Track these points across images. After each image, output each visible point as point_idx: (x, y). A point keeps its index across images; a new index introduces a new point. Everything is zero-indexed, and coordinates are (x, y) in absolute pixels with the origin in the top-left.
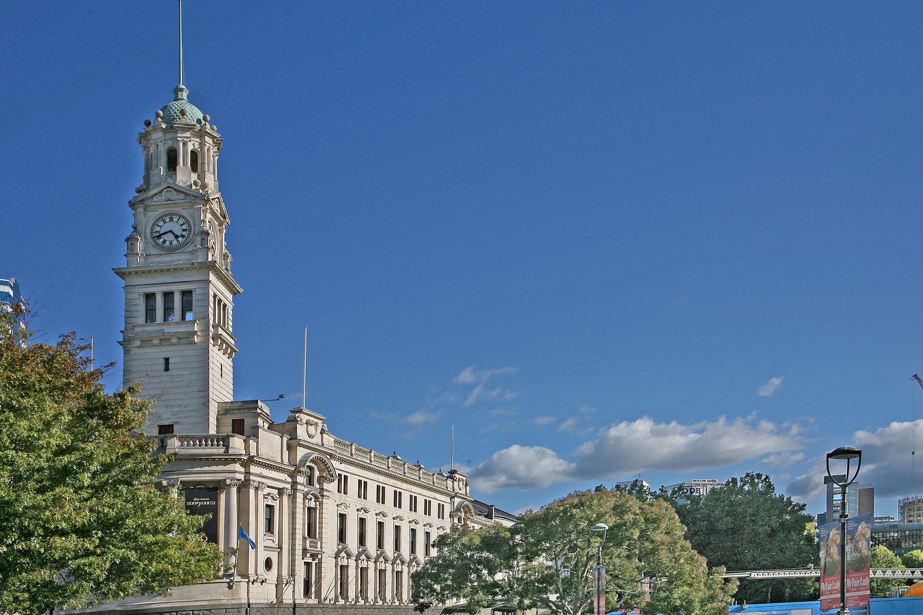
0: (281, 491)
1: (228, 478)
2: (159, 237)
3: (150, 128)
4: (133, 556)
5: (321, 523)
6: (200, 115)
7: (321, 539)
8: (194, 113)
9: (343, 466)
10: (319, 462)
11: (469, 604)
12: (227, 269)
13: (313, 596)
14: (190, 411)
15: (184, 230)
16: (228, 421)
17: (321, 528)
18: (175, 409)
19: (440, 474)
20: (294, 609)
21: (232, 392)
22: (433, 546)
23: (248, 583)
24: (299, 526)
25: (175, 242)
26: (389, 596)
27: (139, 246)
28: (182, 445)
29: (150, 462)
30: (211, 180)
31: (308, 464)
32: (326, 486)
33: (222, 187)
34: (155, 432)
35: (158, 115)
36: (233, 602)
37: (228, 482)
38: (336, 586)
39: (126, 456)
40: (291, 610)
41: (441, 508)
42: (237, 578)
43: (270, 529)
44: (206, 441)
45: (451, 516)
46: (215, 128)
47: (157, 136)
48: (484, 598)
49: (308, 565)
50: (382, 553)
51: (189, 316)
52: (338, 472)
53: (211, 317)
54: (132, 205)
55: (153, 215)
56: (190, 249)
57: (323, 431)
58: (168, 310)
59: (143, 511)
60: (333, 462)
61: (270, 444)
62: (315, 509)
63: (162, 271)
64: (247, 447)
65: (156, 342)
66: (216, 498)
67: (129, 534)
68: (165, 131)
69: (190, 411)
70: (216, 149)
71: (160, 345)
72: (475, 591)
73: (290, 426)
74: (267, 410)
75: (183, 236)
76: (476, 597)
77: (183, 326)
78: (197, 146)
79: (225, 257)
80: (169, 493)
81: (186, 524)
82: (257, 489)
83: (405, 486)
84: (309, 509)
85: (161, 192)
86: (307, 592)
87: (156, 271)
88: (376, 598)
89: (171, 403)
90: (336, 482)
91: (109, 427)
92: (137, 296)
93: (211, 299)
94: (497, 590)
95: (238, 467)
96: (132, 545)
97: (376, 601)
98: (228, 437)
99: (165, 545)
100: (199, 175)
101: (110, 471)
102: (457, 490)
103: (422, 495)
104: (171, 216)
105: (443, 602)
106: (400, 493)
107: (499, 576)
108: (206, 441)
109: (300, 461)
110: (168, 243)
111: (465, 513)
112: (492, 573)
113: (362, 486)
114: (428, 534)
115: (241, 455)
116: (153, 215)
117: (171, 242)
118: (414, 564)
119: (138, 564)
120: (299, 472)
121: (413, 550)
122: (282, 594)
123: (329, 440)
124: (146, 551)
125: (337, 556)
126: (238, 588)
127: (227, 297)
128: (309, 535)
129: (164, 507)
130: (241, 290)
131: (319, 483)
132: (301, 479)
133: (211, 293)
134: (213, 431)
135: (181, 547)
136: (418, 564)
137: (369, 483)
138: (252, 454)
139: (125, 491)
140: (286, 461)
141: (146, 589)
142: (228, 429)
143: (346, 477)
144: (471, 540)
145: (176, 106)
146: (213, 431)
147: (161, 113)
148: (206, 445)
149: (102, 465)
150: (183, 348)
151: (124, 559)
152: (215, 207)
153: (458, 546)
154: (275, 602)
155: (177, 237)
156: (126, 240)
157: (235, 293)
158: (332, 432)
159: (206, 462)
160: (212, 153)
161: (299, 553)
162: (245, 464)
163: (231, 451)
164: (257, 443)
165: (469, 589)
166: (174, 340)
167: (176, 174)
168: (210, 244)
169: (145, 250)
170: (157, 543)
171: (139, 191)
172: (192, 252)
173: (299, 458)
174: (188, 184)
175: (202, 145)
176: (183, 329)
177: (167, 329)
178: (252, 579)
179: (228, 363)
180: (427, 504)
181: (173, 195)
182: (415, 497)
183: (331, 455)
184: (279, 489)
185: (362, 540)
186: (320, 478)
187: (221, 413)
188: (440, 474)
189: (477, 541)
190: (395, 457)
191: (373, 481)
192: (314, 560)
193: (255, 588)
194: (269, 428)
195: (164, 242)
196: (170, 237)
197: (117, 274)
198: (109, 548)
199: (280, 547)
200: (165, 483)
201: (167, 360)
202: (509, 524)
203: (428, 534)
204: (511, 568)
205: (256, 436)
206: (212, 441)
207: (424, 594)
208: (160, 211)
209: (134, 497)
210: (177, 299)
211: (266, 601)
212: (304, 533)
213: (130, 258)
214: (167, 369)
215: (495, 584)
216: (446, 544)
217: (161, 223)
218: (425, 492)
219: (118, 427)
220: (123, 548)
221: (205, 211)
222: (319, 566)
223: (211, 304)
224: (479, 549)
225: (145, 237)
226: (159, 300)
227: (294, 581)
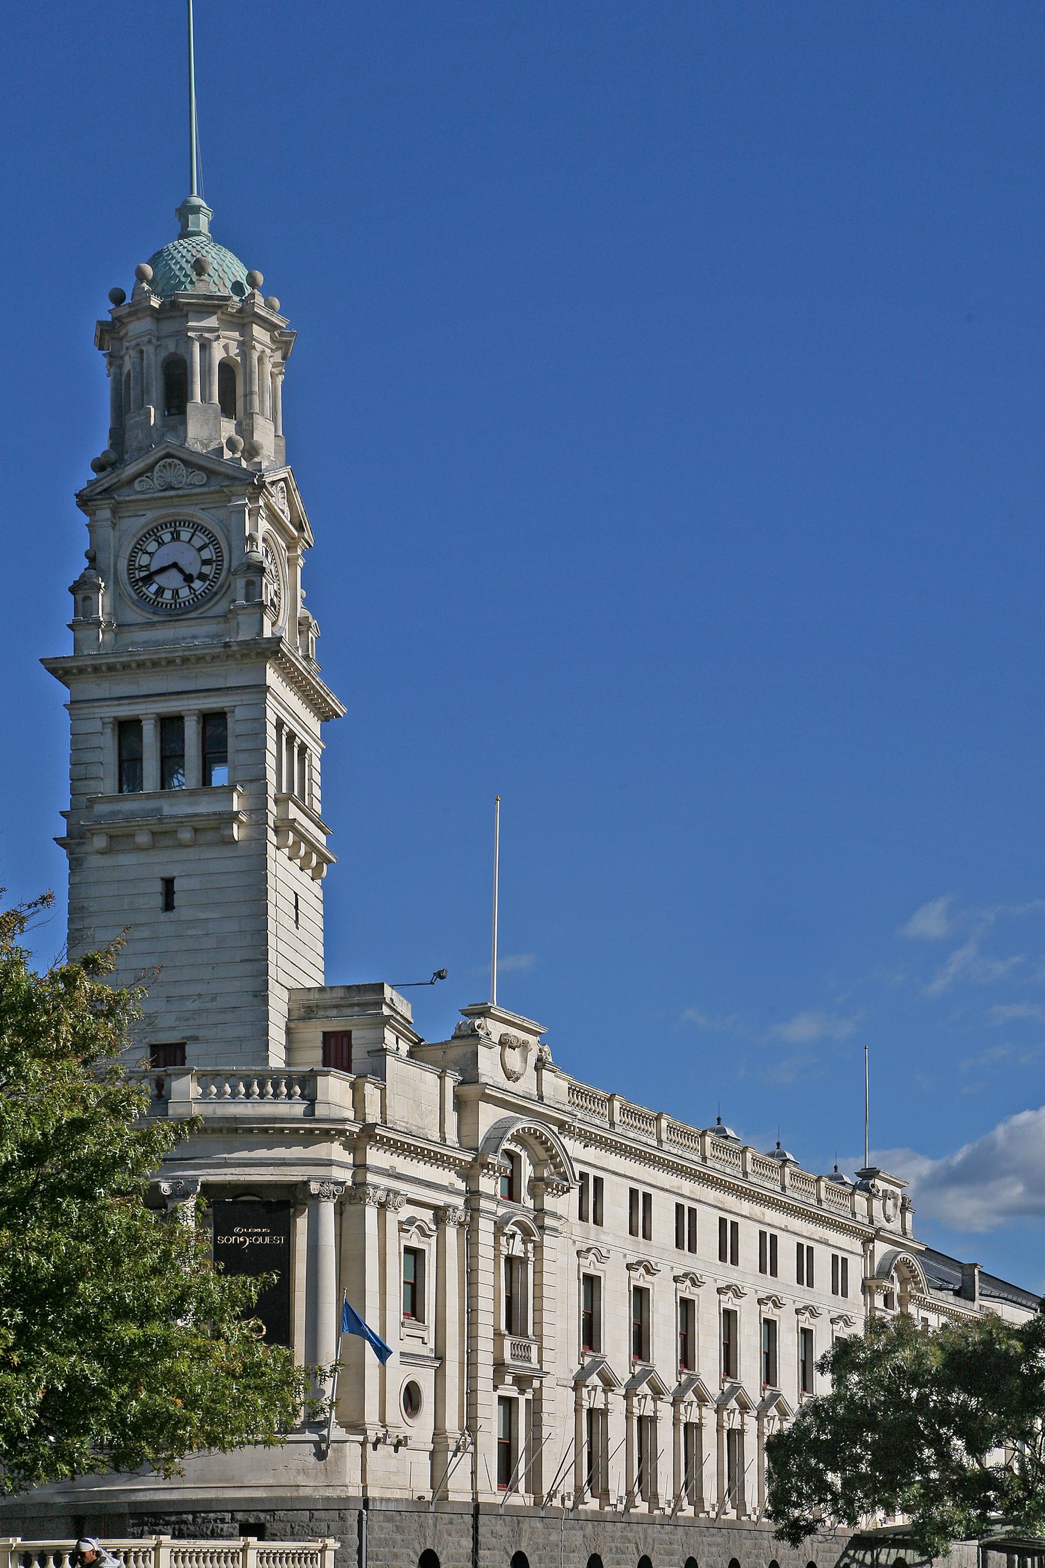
0: (440, 1214)
1: (316, 1179)
2: (148, 579)
3: (123, 310)
4: (94, 1372)
5: (539, 1297)
6: (239, 272)
7: (539, 1337)
8: (227, 269)
9: (591, 1154)
10: (532, 1141)
11: (918, 1528)
12: (306, 657)
13: (522, 1485)
14: (224, 1010)
15: (205, 562)
16: (313, 1033)
17: (538, 1310)
18: (190, 1005)
19: (836, 1178)
20: (476, 1516)
21: (321, 963)
22: (822, 1368)
23: (363, 1444)
24: (485, 1304)
25: (184, 593)
26: (710, 1495)
27: (102, 603)
28: (205, 1094)
29: (132, 1143)
30: (267, 434)
31: (506, 1145)
32: (550, 1202)
33: (292, 455)
34: (142, 1060)
35: (141, 276)
36: (329, 1493)
37: (314, 1188)
38: (577, 1463)
39: (79, 1126)
40: (469, 1519)
41: (840, 1266)
42: (336, 1433)
43: (414, 1309)
44: (262, 1086)
45: (866, 1289)
46: (277, 303)
47: (139, 327)
48: (959, 1516)
49: (507, 1402)
50: (691, 1381)
51: (220, 775)
52: (578, 1168)
53: (271, 776)
54: (84, 501)
55: (134, 525)
56: (221, 608)
57: (540, 1065)
58: (171, 760)
59: (118, 1263)
60: (567, 1142)
61: (413, 1094)
62: (524, 1261)
63: (155, 664)
64: (358, 1102)
65: (143, 839)
66: (287, 1230)
67: (86, 1317)
68: (158, 315)
69: (224, 1010)
70: (278, 357)
71: (153, 847)
72: (932, 1495)
73: (458, 1050)
74: (405, 1008)
75: (202, 577)
76: (935, 1512)
77: (205, 799)
78: (234, 351)
79: (303, 626)
80: (176, 1220)
81: (217, 1297)
82: (382, 1206)
83: (746, 1207)
84: (510, 1260)
85: (151, 468)
86: (506, 1477)
87: (140, 665)
88: (677, 1498)
89: (279, 567)
90: (575, 1193)
91: (38, 1054)
92: (97, 726)
93: (271, 731)
94: (991, 1494)
95: (337, 1151)
96: (92, 1345)
97: (678, 1507)
98: (313, 1075)
99: (167, 1348)
100: (238, 426)
101: (41, 1164)
102: (880, 1221)
103: (792, 1233)
104: (175, 526)
105: (853, 1520)
106: (735, 1225)
107: (995, 1458)
108: (262, 1086)
109: (487, 1139)
110: (168, 595)
111: (903, 1282)
112: (976, 1449)
113: (640, 1204)
114: (806, 1335)
115: (345, 1120)
116: (134, 525)
117: (176, 593)
118: (773, 1411)
119: (107, 1397)
120: (485, 1165)
121: (769, 1375)
122: (445, 1478)
123: (556, 1086)
124: (119, 1362)
125: (578, 1384)
126: (340, 1457)
127: (309, 726)
128: (509, 1326)
129: (166, 1254)
130: (341, 710)
131: (533, 1195)
132: (488, 1184)
133: (271, 717)
134: (277, 1059)
135: (202, 1355)
136: (783, 1414)
137: (657, 1196)
138: (370, 1120)
139: (75, 1211)
140: (452, 1137)
141: (124, 1460)
142: (312, 1057)
143: (598, 1181)
144: (920, 1357)
145: (182, 251)
146: (277, 1059)
147: (149, 270)
148: (262, 1095)
149: (24, 1146)
150: (208, 853)
151: (76, 1383)
152: (279, 502)
153: (885, 1370)
154: (429, 1496)
155: (189, 579)
156: (73, 590)
157: (326, 716)
158: (563, 1066)
159: (263, 1137)
160: (268, 367)
161: (485, 1371)
162: (355, 1145)
163: (320, 1111)
164: (383, 1091)
165: (915, 1490)
166: (186, 835)
167: (184, 423)
168: (268, 594)
169: (114, 612)
170: (146, 1343)
171: (99, 466)
172: (225, 617)
173: (483, 1130)
174: (213, 446)
175: (246, 346)
176: (205, 806)
177: (171, 808)
178: (372, 1436)
179: (311, 891)
180: (804, 1256)
181: (179, 474)
182: (774, 1238)
183: (561, 1124)
184: (436, 1208)
185: (640, 1346)
186: (536, 1181)
187: (296, 1014)
188: (836, 1178)
189: (934, 1361)
190: (720, 1132)
191: (667, 1192)
192: (522, 1391)
193: (380, 1459)
194: (411, 1054)
195: (160, 591)
196: (172, 580)
197: (53, 671)
198: (39, 1354)
199: (440, 1357)
200: (165, 1187)
201: (169, 883)
202: (1019, 1317)
203: (806, 1335)
204: (1026, 1435)
205: (380, 1073)
206: (276, 1086)
207: (800, 1495)
208: (150, 515)
209: (98, 1227)
210: (191, 730)
211: (405, 1495)
212: (497, 1320)
213: (82, 634)
214: (169, 906)
215: (987, 1479)
216: (856, 1367)
217: (152, 547)
218: (797, 1224)
219: (60, 1054)
220: (71, 1352)
221: (255, 513)
222: (535, 1408)
223: (271, 745)
224: (944, 1382)
225: (116, 582)
226: (150, 733)
227: (474, 1443)
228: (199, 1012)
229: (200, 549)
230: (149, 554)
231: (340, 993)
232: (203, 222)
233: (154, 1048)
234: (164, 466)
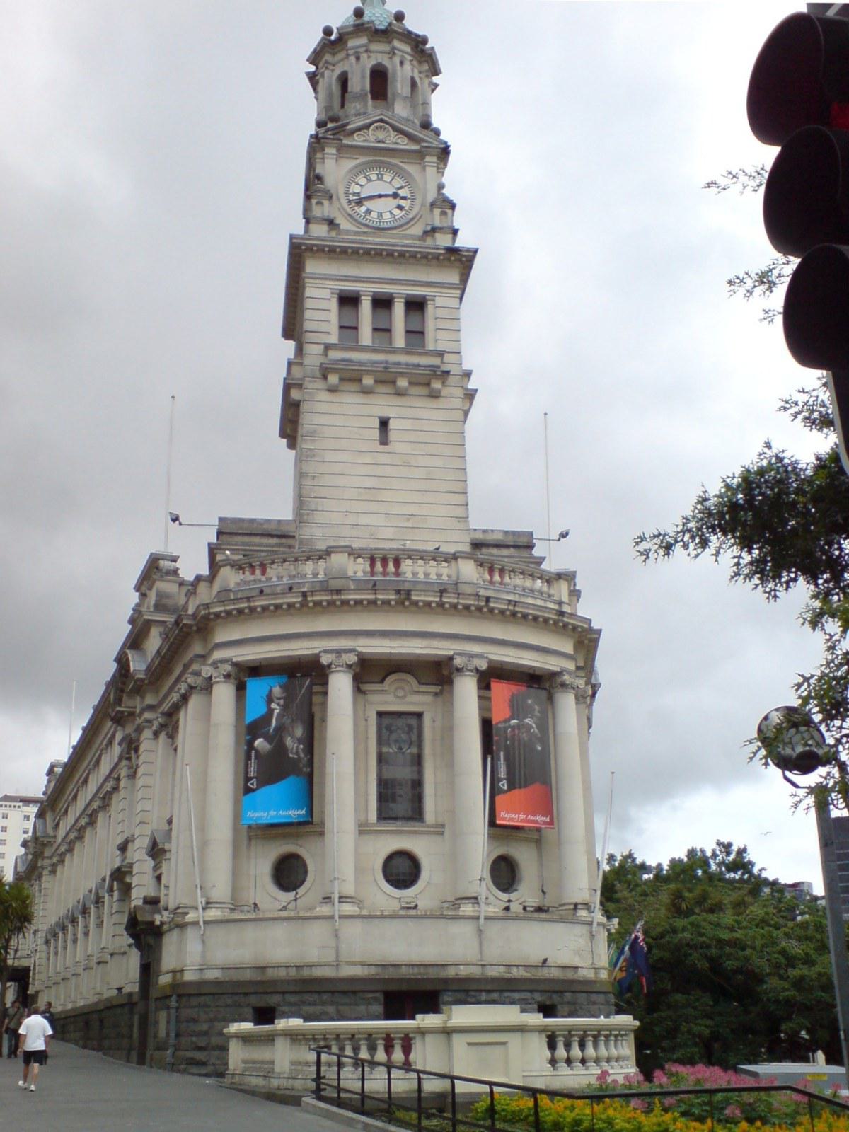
2: (359, 202)
85: (367, 127)
110: (374, 215)
195: (368, 212)
214: (384, 441)
229: (369, 180)
230: (361, 185)
234: (377, 128)
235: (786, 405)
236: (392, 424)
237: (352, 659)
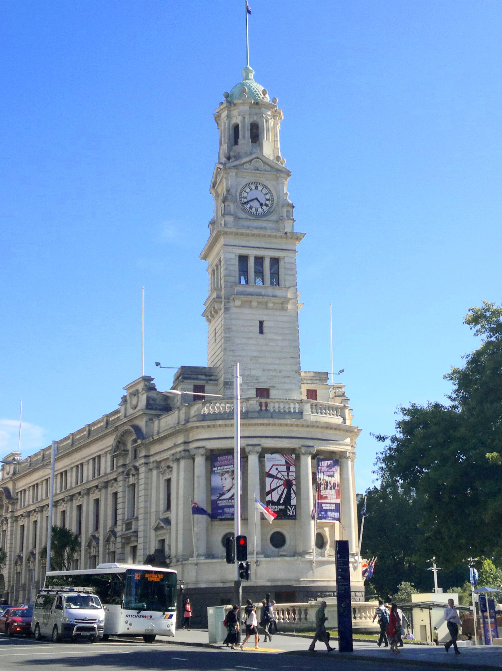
2: (246, 203)
14: (285, 377)
15: (268, 200)
18: (272, 373)
25: (260, 210)
37: (303, 450)
69: (285, 377)
75: (266, 205)
85: (251, 161)
110: (254, 209)
117: (257, 209)
155: (261, 205)
195: (251, 208)
196: (255, 204)
214: (261, 332)
228: (275, 377)
230: (247, 193)
231: (312, 374)
232: (251, 76)
233: (257, 389)
235: (445, 377)
236: (265, 324)
237: (259, 449)
